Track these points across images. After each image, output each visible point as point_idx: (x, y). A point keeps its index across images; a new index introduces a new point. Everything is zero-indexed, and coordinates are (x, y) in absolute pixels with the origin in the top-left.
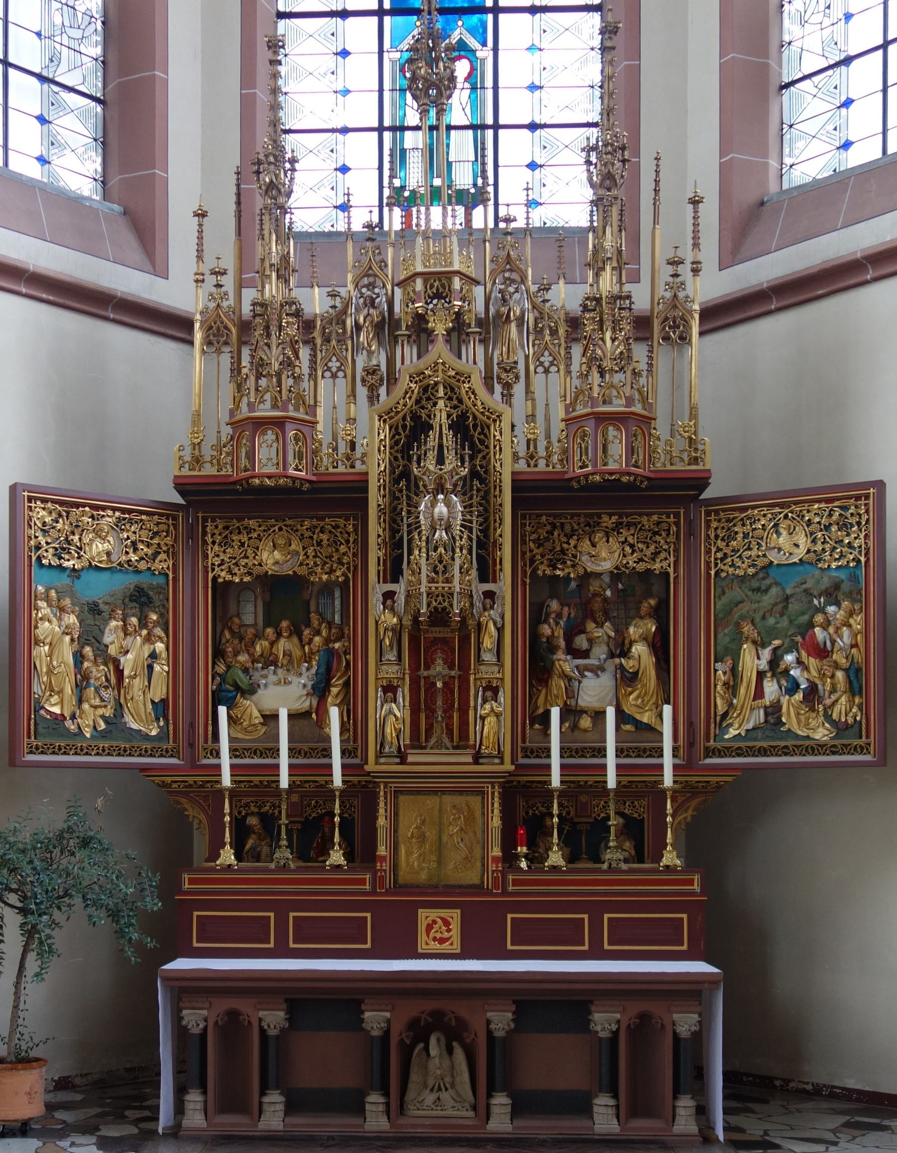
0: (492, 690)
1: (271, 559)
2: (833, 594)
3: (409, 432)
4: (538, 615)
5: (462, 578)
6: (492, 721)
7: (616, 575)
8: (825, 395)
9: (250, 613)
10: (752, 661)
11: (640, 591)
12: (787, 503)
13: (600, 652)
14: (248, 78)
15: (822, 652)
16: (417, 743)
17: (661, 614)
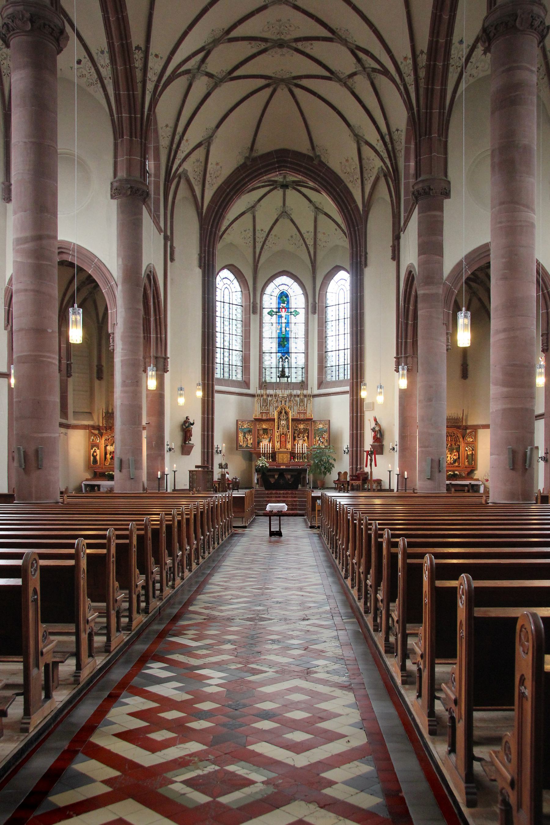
0: (289, 442)
1: (264, 427)
2: (325, 432)
3: (280, 413)
4: (294, 433)
5: (285, 429)
6: (289, 446)
7: (303, 429)
8: (327, 408)
9: (261, 432)
10: (317, 438)
11: (306, 430)
12: (320, 421)
13: (301, 437)
14: (260, 376)
15: (324, 438)
16: (280, 448)
17: (308, 433)
